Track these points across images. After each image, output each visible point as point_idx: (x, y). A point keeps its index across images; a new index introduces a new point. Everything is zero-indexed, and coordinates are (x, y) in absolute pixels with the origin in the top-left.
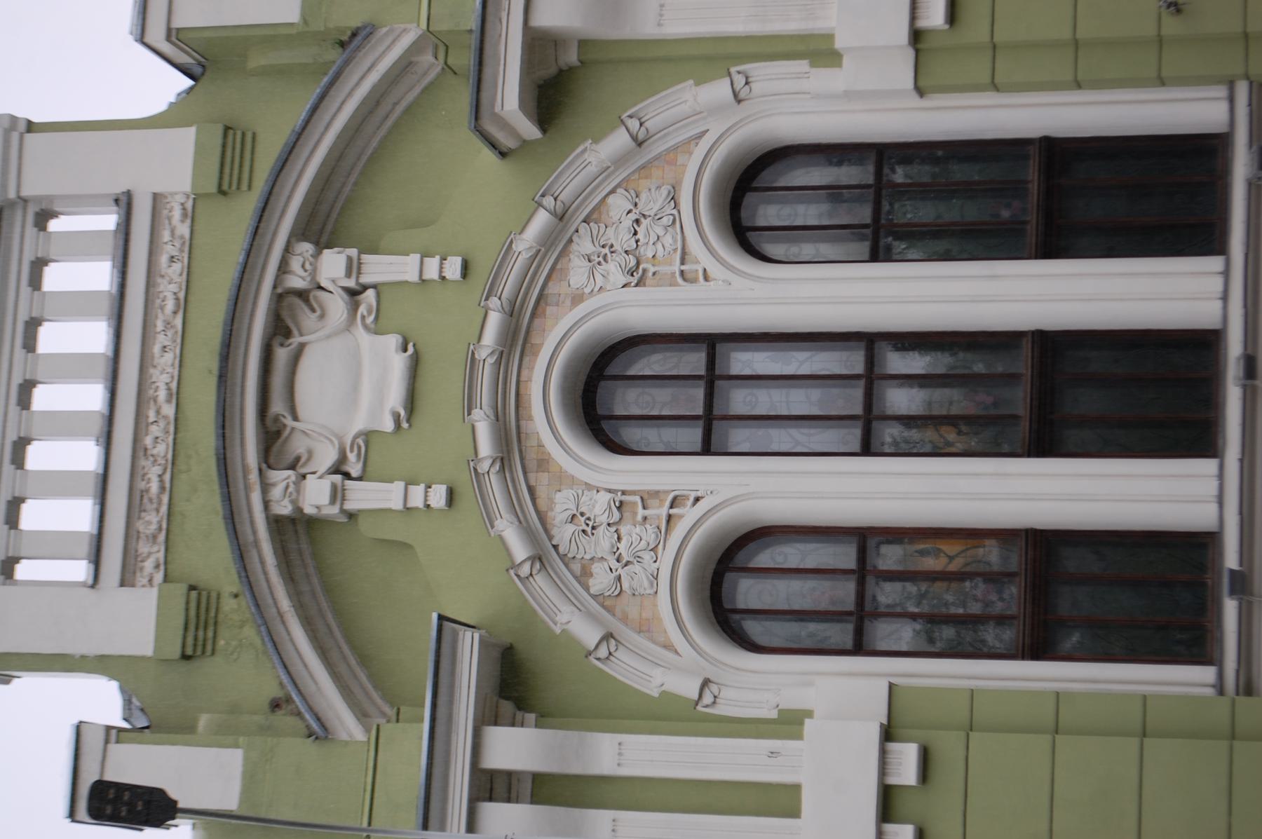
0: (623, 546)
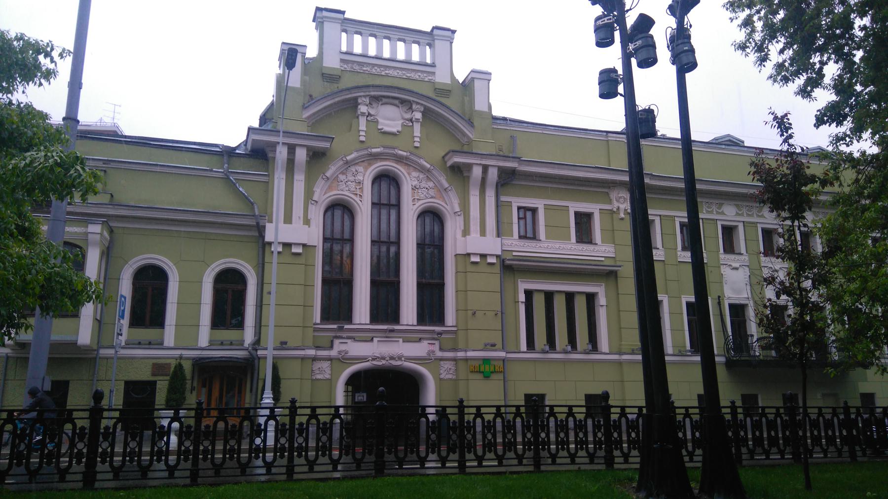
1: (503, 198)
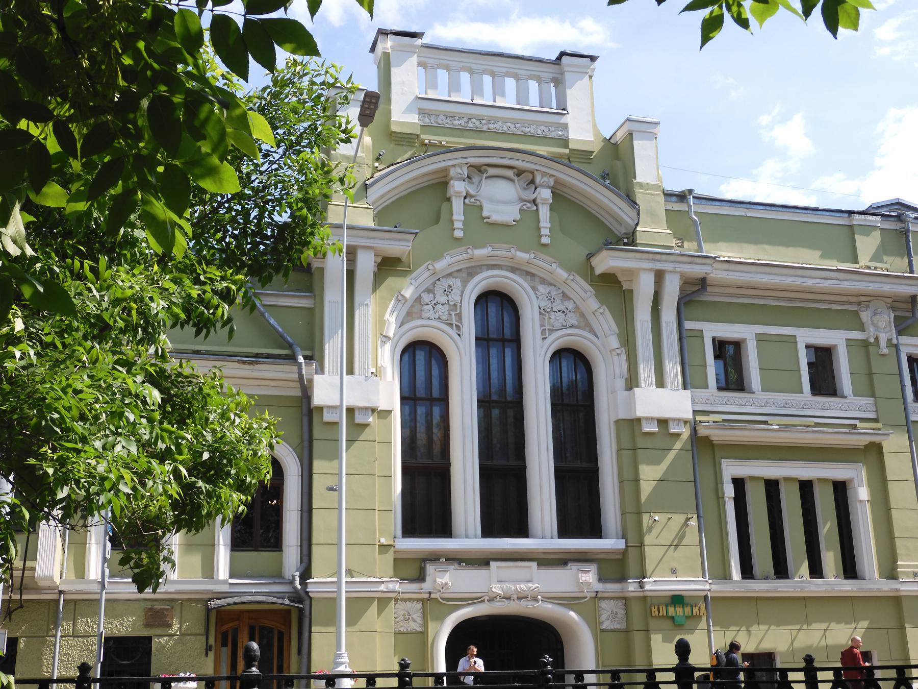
0: (440, 306)
1: (689, 325)
